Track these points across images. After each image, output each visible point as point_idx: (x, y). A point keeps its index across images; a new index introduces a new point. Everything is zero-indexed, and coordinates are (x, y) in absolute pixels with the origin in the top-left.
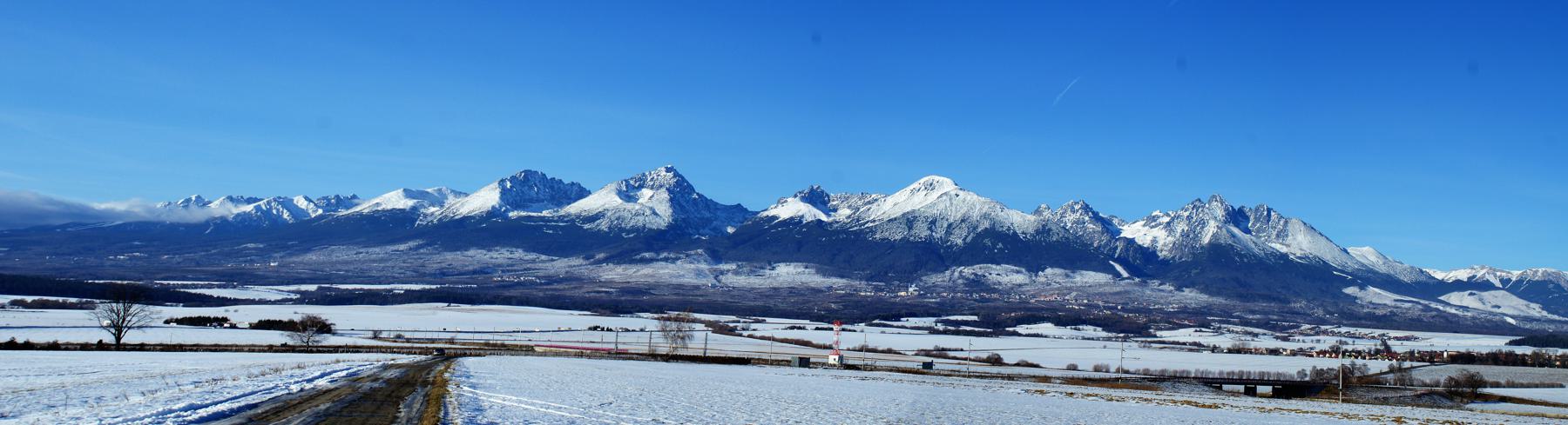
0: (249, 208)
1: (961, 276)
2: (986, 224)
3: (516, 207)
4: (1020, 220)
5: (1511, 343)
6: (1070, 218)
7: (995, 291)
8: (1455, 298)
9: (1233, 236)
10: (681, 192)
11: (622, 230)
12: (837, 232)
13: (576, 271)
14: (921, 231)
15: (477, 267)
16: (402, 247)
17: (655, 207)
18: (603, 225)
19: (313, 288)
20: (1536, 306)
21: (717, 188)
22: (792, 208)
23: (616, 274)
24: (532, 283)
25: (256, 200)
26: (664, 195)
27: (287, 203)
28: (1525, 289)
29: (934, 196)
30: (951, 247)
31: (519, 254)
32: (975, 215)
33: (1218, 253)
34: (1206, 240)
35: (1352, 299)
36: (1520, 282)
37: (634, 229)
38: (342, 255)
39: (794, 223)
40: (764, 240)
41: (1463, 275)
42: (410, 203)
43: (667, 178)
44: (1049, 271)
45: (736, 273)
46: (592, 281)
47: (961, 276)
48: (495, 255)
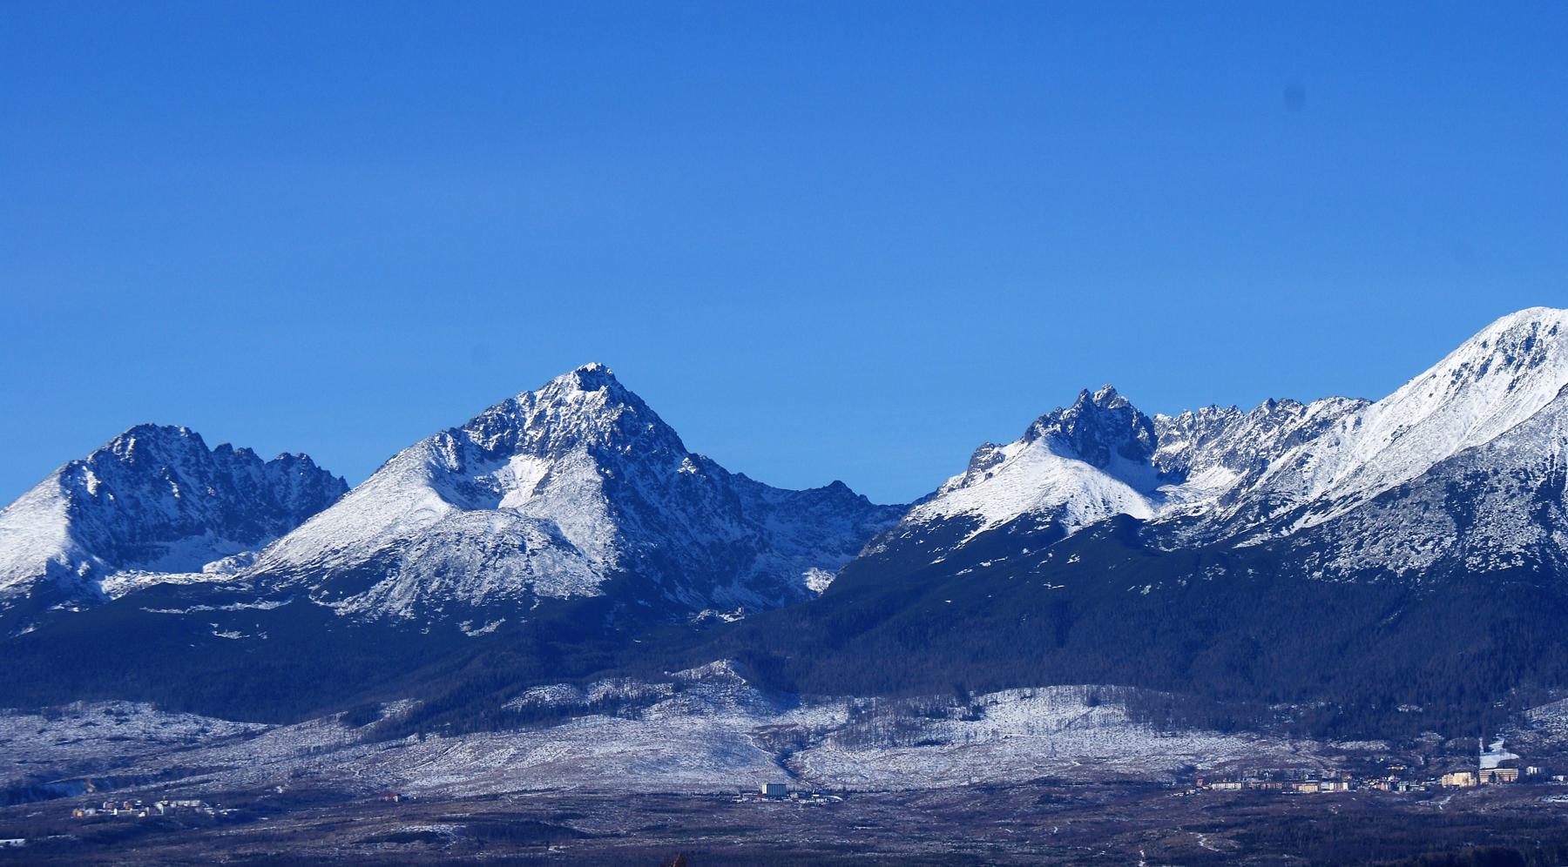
3: (122, 557)
10: (637, 457)
11: (458, 610)
12: (1193, 558)
13: (325, 769)
14: (1510, 531)
15: (20, 775)
17: (556, 517)
21: (761, 434)
22: (1027, 482)
24: (192, 820)
26: (583, 473)
31: (144, 720)
37: (499, 605)
39: (1037, 534)
45: (850, 738)
48: (70, 729)
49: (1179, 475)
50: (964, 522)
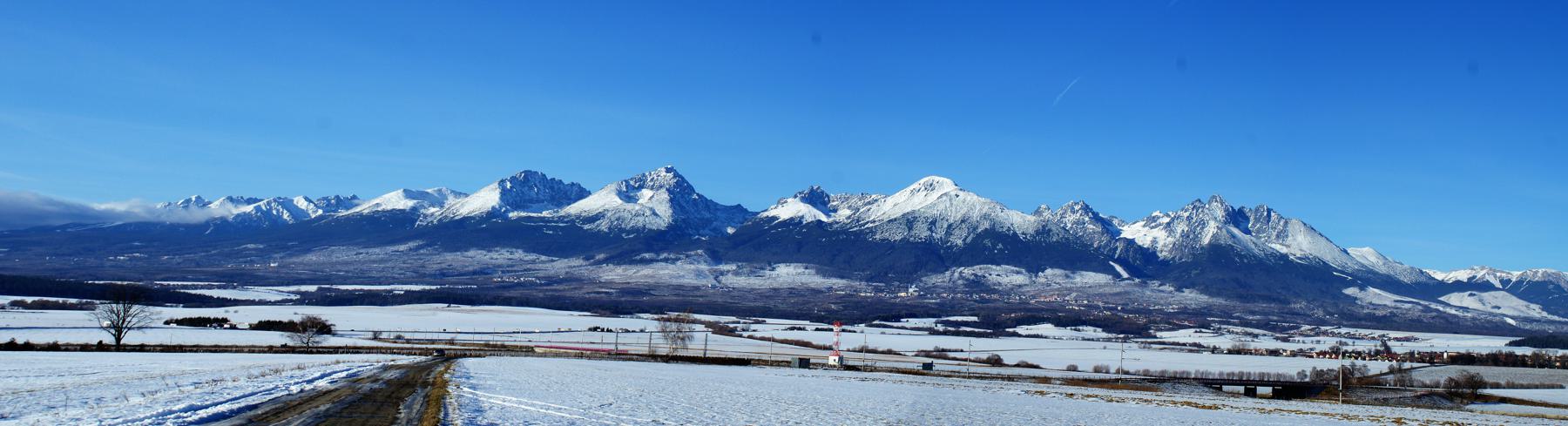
0: (249, 208)
1: (961, 277)
2: (986, 225)
3: (516, 207)
4: (1020, 221)
5: (1511, 344)
6: (1070, 219)
7: (995, 291)
8: (1455, 299)
9: (1233, 236)
10: (681, 193)
11: (622, 230)
12: (837, 233)
13: (576, 272)
14: (921, 232)
15: (477, 267)
16: (402, 248)
17: (655, 207)
18: (603, 226)
19: (313, 288)
20: (1536, 307)
21: (717, 189)
22: (792, 209)
23: (616, 274)
24: (532, 284)
25: (256, 200)
26: (664, 195)
27: (287, 204)
28: (1525, 290)
29: (934, 196)
30: (951, 247)
31: (519, 254)
32: (975, 215)
33: (1218, 253)
34: (1206, 241)
35: (1352, 300)
36: (1520, 282)
37: (634, 230)
38: (342, 255)
39: (794, 223)
40: (764, 241)
41: (1463, 275)
42: (410, 203)
43: (667, 178)
44: (1049, 271)
45: (736, 273)
46: (592, 282)
47: (961, 277)
48: (495, 255)
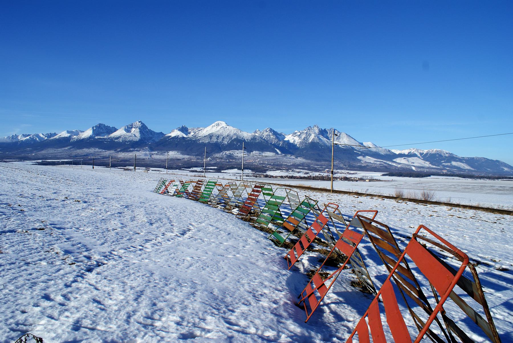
0: (28, 138)
1: (226, 154)
2: (235, 137)
3: (97, 135)
4: (247, 135)
5: (383, 175)
6: (265, 134)
7: (235, 159)
8: (398, 160)
9: (320, 139)
10: (143, 129)
11: (126, 141)
12: (188, 140)
13: (112, 155)
14: (214, 140)
15: (85, 154)
16: (66, 148)
17: (135, 134)
18: (121, 140)
19: (40, 161)
20: (428, 163)
21: (155, 127)
22: (176, 133)
23: (122, 155)
24: (99, 158)
25: (30, 135)
26: (138, 130)
27: (38, 136)
28: (426, 157)
29: (219, 128)
30: (223, 145)
31: (97, 150)
32: (232, 134)
33: (314, 145)
34: (310, 141)
35: (360, 161)
36: (427, 154)
37: (130, 141)
38: (51, 151)
39: (176, 138)
40: (164, 143)
41: (406, 152)
42: (69, 135)
43: (139, 124)
44: (254, 152)
45: (157, 154)
46: (115, 158)
47: (226, 154)
48: (90, 150)
49: (190, 133)
50: (170, 136)
